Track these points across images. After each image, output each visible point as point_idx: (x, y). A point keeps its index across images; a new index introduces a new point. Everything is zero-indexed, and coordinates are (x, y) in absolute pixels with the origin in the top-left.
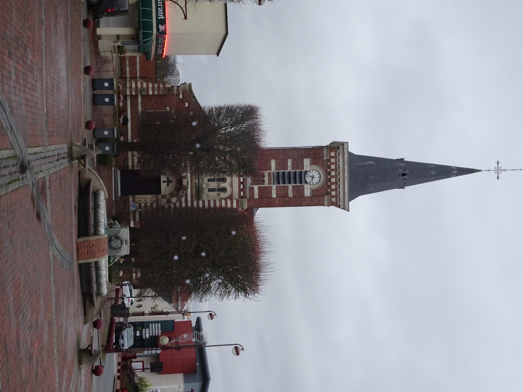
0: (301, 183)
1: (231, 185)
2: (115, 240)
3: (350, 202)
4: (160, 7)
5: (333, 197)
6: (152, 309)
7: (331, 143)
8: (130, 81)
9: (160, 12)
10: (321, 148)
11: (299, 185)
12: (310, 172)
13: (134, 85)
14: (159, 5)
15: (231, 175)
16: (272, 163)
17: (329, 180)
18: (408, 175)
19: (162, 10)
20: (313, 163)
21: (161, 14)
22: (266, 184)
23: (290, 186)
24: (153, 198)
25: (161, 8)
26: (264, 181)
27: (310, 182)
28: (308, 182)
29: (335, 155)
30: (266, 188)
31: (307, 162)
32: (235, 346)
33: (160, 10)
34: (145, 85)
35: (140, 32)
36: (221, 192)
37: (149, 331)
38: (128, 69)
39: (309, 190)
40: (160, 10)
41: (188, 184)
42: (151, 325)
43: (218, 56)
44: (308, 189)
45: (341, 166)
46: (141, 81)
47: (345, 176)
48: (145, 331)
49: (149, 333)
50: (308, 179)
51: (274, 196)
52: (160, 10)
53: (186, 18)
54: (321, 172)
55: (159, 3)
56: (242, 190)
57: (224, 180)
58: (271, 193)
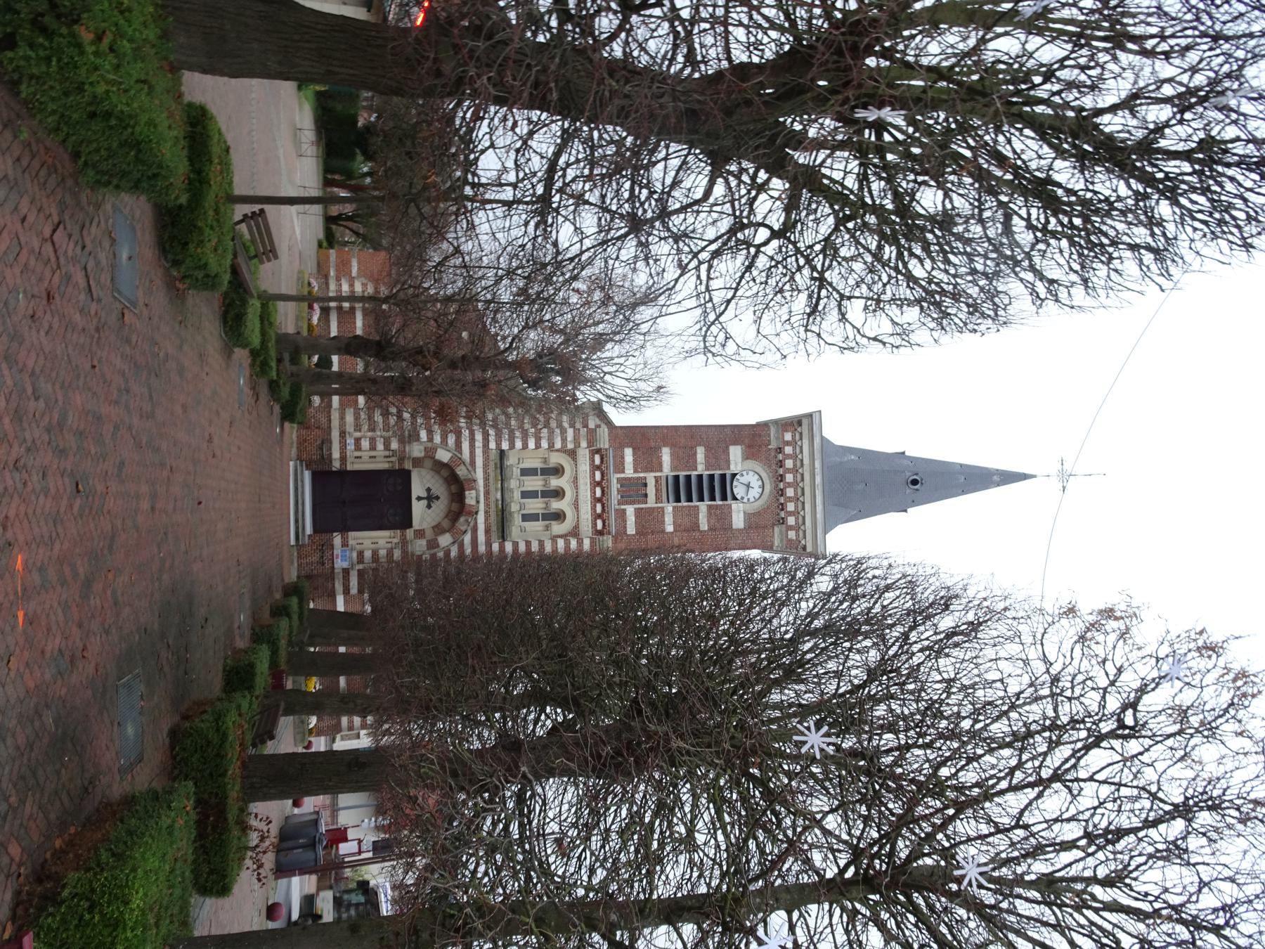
28: (738, 497)
54: (764, 475)
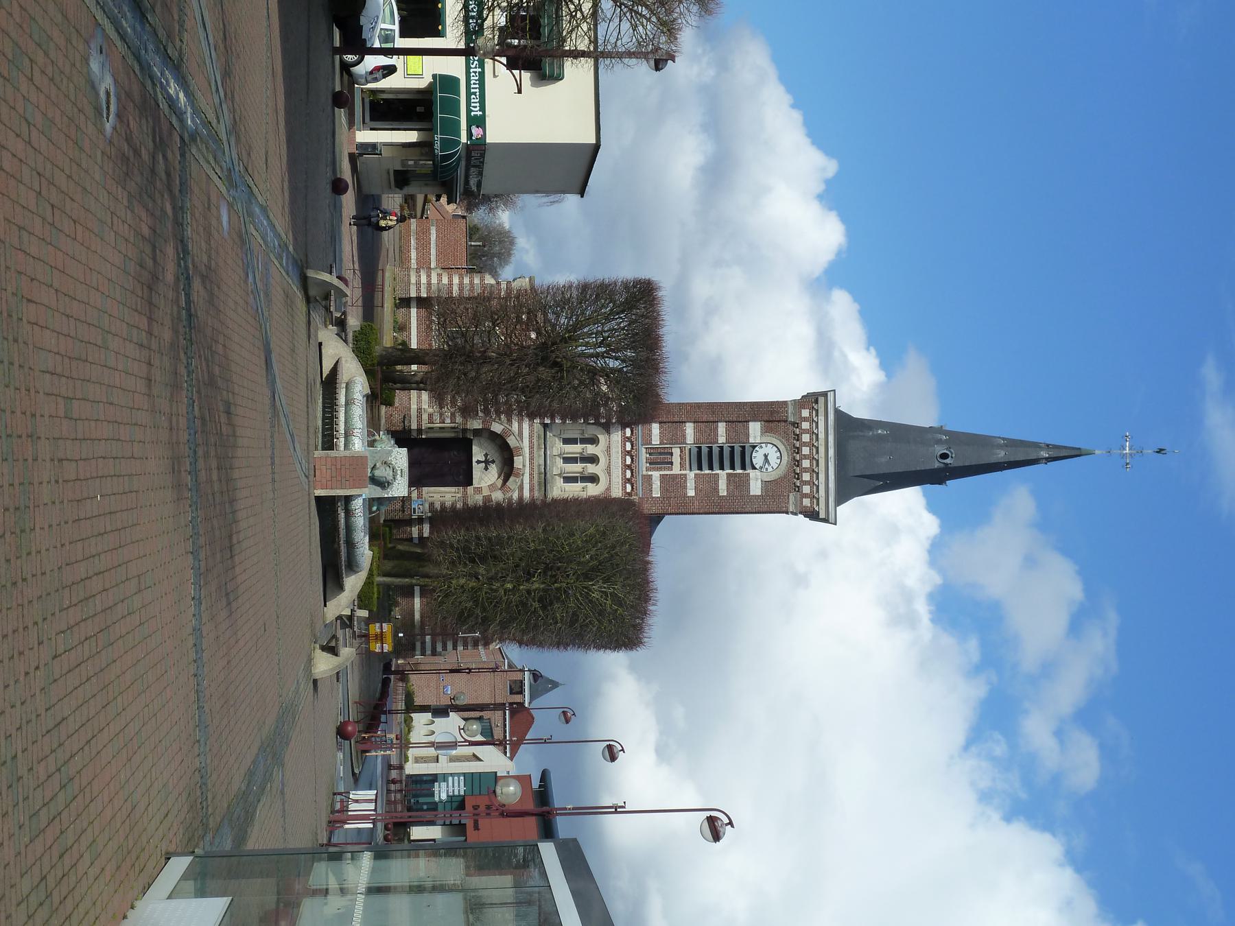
0: (743, 467)
1: (608, 471)
2: (382, 468)
3: (838, 508)
4: (475, 93)
5: (806, 496)
6: (452, 701)
7: (803, 397)
8: (418, 271)
9: (473, 88)
10: (785, 403)
11: (741, 471)
12: (761, 447)
13: (424, 279)
14: (472, 90)
15: (607, 428)
16: (687, 428)
17: (798, 463)
18: (952, 457)
19: (477, 100)
20: (765, 431)
21: (476, 107)
22: (676, 470)
23: (723, 475)
24: (458, 493)
25: (476, 96)
26: (672, 463)
27: (761, 468)
28: (757, 467)
29: (810, 415)
30: (675, 477)
31: (755, 428)
32: (608, 743)
33: (474, 98)
34: (445, 280)
35: (436, 139)
36: (589, 485)
37: (448, 787)
38: (413, 255)
39: (759, 482)
40: (475, 100)
41: (524, 466)
42: (450, 779)
43: (582, 196)
44: (757, 479)
45: (822, 436)
46: (440, 271)
47: (830, 456)
48: (440, 787)
49: (448, 791)
50: (758, 459)
51: (691, 493)
52: (474, 98)
53: (520, 91)
54: (782, 447)
55: (472, 86)
56: (629, 481)
57: (594, 441)
58: (685, 487)
